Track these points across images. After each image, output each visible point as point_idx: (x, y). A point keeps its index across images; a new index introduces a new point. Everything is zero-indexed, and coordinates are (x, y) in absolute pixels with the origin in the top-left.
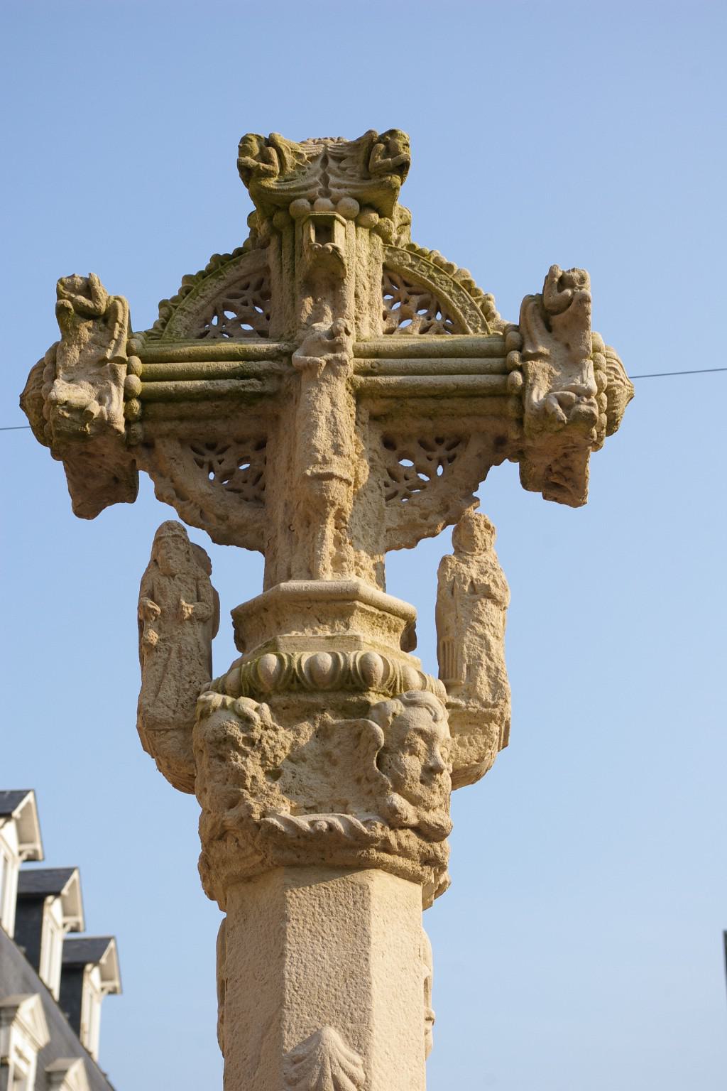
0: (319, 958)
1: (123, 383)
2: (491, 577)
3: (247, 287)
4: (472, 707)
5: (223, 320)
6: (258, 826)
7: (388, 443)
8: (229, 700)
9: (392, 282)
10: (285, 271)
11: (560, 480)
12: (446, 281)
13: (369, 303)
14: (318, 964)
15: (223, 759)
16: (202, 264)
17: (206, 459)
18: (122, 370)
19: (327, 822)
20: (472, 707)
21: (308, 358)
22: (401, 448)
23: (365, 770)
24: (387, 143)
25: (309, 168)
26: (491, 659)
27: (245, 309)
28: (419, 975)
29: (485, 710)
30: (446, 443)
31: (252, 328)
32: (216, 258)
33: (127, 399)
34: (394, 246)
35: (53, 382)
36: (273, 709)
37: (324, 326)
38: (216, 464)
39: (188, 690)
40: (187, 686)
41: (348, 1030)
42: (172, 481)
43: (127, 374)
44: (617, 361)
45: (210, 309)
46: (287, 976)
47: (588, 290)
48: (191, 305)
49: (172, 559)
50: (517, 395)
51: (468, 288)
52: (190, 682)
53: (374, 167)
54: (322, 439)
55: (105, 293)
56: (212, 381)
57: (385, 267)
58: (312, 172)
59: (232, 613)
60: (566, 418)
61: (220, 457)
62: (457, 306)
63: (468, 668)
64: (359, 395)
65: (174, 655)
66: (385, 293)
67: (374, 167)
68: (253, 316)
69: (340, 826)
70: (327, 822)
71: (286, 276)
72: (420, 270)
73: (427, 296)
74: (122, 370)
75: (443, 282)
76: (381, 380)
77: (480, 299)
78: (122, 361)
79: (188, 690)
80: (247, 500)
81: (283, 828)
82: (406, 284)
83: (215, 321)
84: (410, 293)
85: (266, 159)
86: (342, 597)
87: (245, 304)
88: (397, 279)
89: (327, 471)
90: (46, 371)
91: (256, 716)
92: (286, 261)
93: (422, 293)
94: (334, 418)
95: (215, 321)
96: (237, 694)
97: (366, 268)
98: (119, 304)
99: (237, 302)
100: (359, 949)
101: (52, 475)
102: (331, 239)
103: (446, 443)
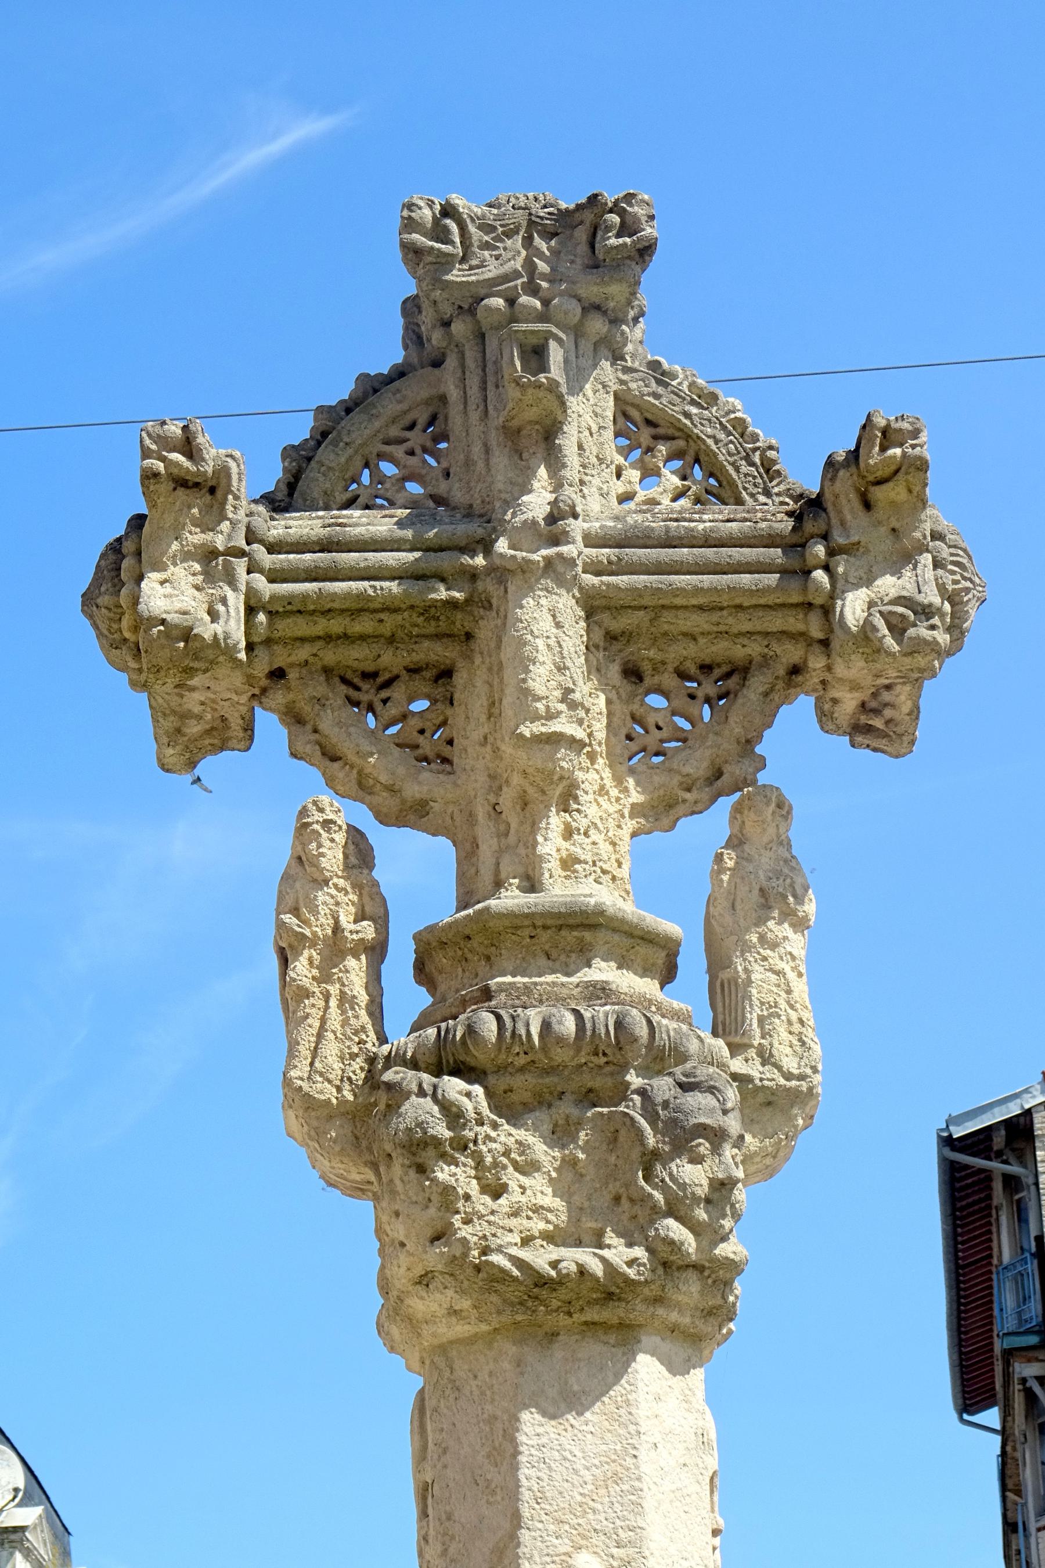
0: (569, 1457)
1: (243, 588)
2: (788, 881)
3: (411, 427)
4: (768, 1080)
5: (379, 478)
6: (478, 1269)
7: (633, 673)
8: (427, 1078)
9: (626, 416)
10: (471, 407)
11: (876, 725)
12: (709, 421)
13: (597, 457)
14: (567, 1464)
15: (422, 1169)
16: (342, 390)
17: (364, 698)
18: (241, 566)
19: (577, 1263)
20: (768, 1080)
21: (519, 554)
22: (648, 681)
23: (627, 1186)
24: (623, 214)
25: (505, 249)
26: (792, 1007)
27: (412, 461)
28: (703, 1471)
29: (788, 1084)
30: (717, 672)
31: (422, 491)
32: (363, 379)
33: (251, 611)
34: (629, 364)
35: (139, 585)
36: (489, 1094)
37: (537, 502)
38: (378, 706)
39: (357, 1055)
40: (355, 1050)
41: (613, 1557)
42: (316, 731)
43: (248, 573)
44: (965, 551)
45: (359, 462)
46: (524, 1482)
47: (926, 447)
48: (332, 456)
49: (324, 856)
50: (822, 606)
51: (740, 430)
52: (359, 1043)
53: (596, 246)
54: (541, 679)
55: (213, 453)
56: (372, 583)
57: (617, 397)
58: (510, 255)
59: (414, 938)
60: (897, 648)
61: (384, 694)
62: (726, 460)
63: (761, 1020)
64: (593, 607)
65: (333, 1003)
66: (617, 435)
67: (596, 246)
68: (424, 472)
69: (597, 1268)
70: (577, 1263)
71: (474, 416)
72: (671, 403)
73: (681, 443)
74: (241, 566)
75: (704, 422)
76: (622, 580)
77: (758, 448)
78: (242, 554)
79: (357, 1055)
80: (426, 759)
81: (516, 1272)
82: (649, 422)
83: (366, 477)
84: (656, 438)
85: (440, 234)
86: (578, 921)
87: (411, 453)
88: (635, 414)
89: (553, 729)
90: (122, 562)
91: (468, 1105)
92: (474, 392)
93: (673, 438)
94: (560, 646)
95: (366, 477)
96: (438, 1073)
97: (592, 402)
98: (232, 465)
99: (398, 451)
100: (625, 1442)
101: (128, 713)
102: (544, 368)
103: (717, 672)
